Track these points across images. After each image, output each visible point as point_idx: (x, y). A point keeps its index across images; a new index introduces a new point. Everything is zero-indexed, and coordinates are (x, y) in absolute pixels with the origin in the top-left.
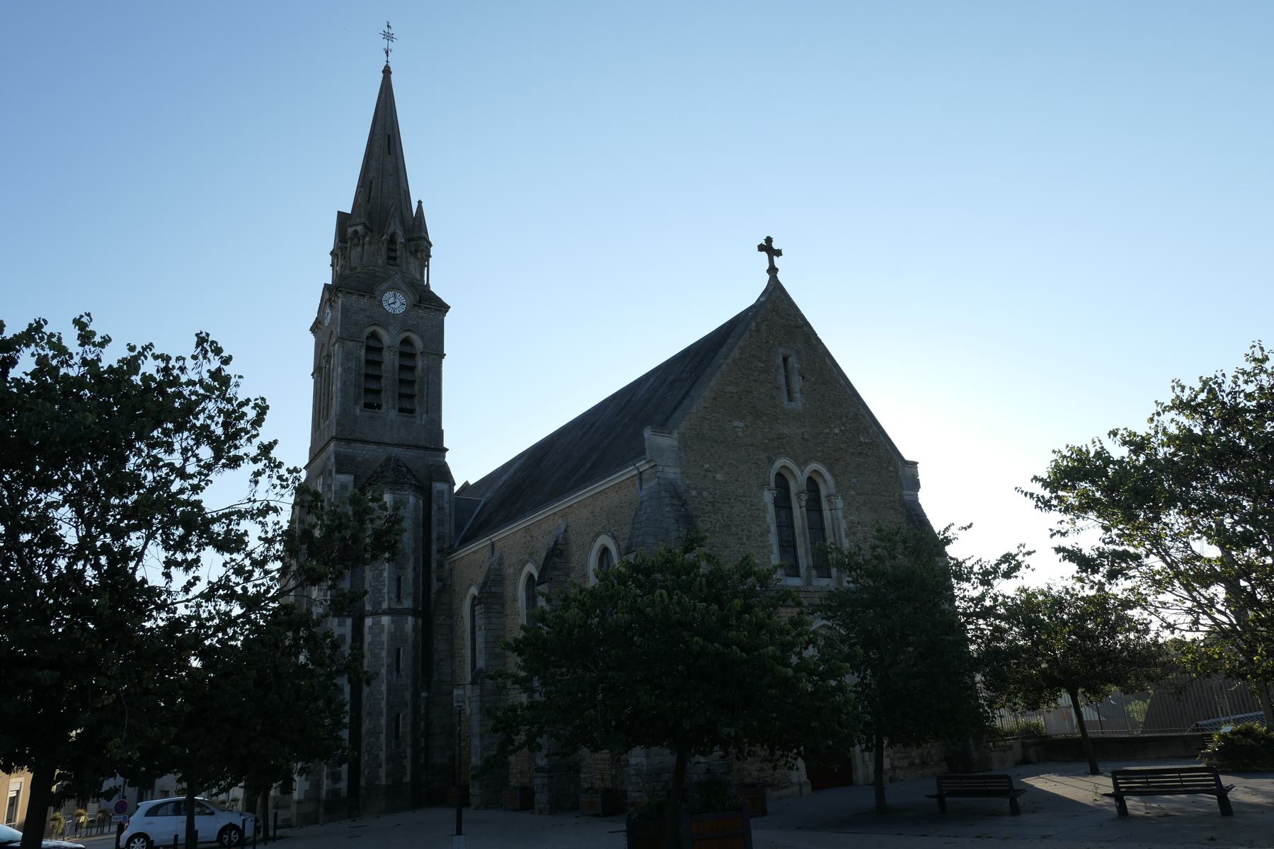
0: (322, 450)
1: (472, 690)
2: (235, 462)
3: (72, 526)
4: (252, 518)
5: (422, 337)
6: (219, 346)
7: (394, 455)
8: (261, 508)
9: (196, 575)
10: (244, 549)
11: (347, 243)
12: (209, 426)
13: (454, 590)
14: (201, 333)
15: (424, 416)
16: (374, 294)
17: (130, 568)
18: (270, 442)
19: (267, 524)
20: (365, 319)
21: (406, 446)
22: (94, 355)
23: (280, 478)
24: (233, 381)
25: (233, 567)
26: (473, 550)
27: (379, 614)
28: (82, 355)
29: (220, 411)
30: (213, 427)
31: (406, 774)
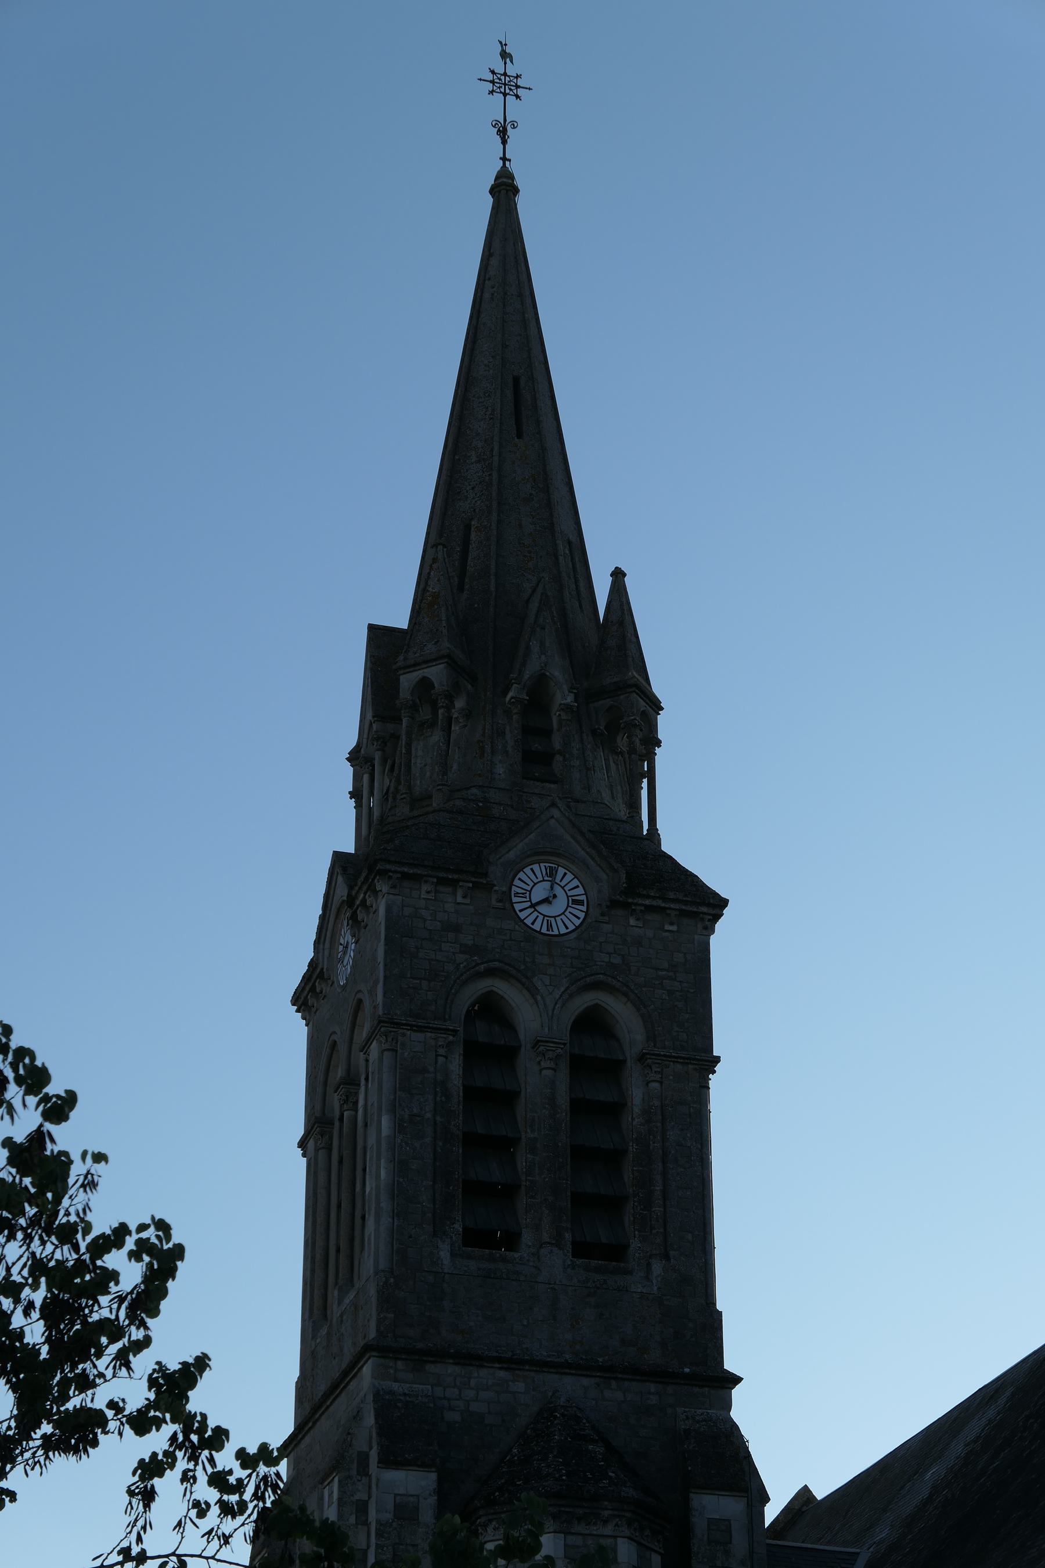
6: (38, 1063)
7: (562, 1401)
11: (399, 720)
15: (657, 1268)
16: (485, 875)
18: (185, 1364)
20: (460, 958)
24: (77, 1170)
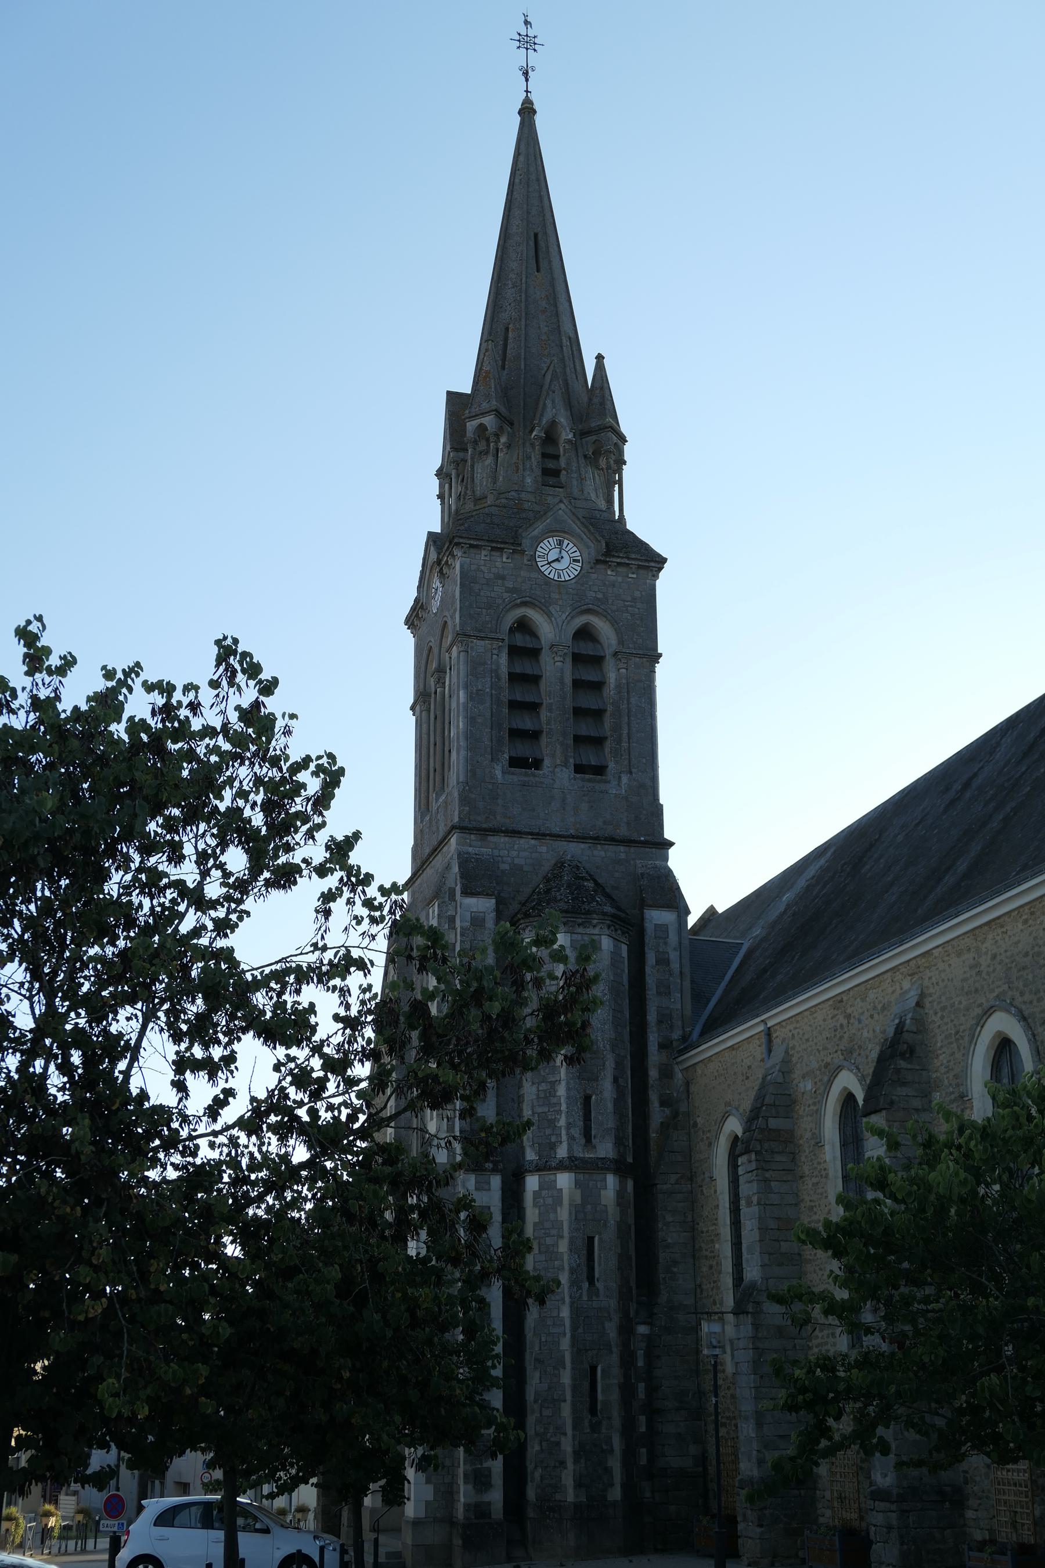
0: (435, 851)
1: (737, 1326)
2: (286, 877)
3: (24, 996)
4: (320, 981)
5: (613, 622)
6: (255, 661)
8: (336, 961)
9: (227, 1086)
10: (309, 1039)
12: (240, 810)
13: (695, 1124)
14: (225, 638)
15: (625, 779)
16: (520, 545)
17: (120, 1072)
19: (349, 991)
20: (506, 595)
21: (591, 838)
22: (50, 689)
23: (368, 903)
24: (280, 724)
25: (291, 1072)
26: (730, 1043)
27: (550, 1169)
28: (31, 691)
29: (258, 781)
30: (247, 812)
31: (612, 1485)
